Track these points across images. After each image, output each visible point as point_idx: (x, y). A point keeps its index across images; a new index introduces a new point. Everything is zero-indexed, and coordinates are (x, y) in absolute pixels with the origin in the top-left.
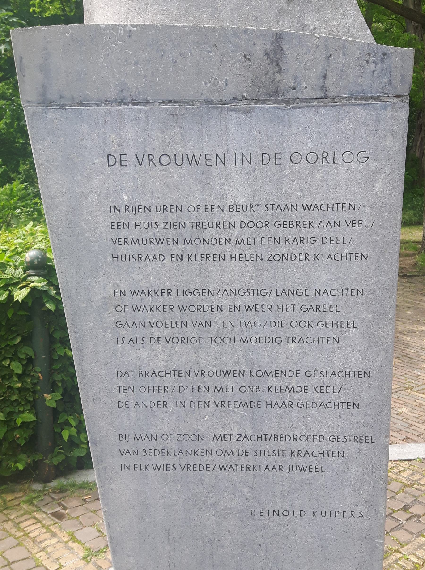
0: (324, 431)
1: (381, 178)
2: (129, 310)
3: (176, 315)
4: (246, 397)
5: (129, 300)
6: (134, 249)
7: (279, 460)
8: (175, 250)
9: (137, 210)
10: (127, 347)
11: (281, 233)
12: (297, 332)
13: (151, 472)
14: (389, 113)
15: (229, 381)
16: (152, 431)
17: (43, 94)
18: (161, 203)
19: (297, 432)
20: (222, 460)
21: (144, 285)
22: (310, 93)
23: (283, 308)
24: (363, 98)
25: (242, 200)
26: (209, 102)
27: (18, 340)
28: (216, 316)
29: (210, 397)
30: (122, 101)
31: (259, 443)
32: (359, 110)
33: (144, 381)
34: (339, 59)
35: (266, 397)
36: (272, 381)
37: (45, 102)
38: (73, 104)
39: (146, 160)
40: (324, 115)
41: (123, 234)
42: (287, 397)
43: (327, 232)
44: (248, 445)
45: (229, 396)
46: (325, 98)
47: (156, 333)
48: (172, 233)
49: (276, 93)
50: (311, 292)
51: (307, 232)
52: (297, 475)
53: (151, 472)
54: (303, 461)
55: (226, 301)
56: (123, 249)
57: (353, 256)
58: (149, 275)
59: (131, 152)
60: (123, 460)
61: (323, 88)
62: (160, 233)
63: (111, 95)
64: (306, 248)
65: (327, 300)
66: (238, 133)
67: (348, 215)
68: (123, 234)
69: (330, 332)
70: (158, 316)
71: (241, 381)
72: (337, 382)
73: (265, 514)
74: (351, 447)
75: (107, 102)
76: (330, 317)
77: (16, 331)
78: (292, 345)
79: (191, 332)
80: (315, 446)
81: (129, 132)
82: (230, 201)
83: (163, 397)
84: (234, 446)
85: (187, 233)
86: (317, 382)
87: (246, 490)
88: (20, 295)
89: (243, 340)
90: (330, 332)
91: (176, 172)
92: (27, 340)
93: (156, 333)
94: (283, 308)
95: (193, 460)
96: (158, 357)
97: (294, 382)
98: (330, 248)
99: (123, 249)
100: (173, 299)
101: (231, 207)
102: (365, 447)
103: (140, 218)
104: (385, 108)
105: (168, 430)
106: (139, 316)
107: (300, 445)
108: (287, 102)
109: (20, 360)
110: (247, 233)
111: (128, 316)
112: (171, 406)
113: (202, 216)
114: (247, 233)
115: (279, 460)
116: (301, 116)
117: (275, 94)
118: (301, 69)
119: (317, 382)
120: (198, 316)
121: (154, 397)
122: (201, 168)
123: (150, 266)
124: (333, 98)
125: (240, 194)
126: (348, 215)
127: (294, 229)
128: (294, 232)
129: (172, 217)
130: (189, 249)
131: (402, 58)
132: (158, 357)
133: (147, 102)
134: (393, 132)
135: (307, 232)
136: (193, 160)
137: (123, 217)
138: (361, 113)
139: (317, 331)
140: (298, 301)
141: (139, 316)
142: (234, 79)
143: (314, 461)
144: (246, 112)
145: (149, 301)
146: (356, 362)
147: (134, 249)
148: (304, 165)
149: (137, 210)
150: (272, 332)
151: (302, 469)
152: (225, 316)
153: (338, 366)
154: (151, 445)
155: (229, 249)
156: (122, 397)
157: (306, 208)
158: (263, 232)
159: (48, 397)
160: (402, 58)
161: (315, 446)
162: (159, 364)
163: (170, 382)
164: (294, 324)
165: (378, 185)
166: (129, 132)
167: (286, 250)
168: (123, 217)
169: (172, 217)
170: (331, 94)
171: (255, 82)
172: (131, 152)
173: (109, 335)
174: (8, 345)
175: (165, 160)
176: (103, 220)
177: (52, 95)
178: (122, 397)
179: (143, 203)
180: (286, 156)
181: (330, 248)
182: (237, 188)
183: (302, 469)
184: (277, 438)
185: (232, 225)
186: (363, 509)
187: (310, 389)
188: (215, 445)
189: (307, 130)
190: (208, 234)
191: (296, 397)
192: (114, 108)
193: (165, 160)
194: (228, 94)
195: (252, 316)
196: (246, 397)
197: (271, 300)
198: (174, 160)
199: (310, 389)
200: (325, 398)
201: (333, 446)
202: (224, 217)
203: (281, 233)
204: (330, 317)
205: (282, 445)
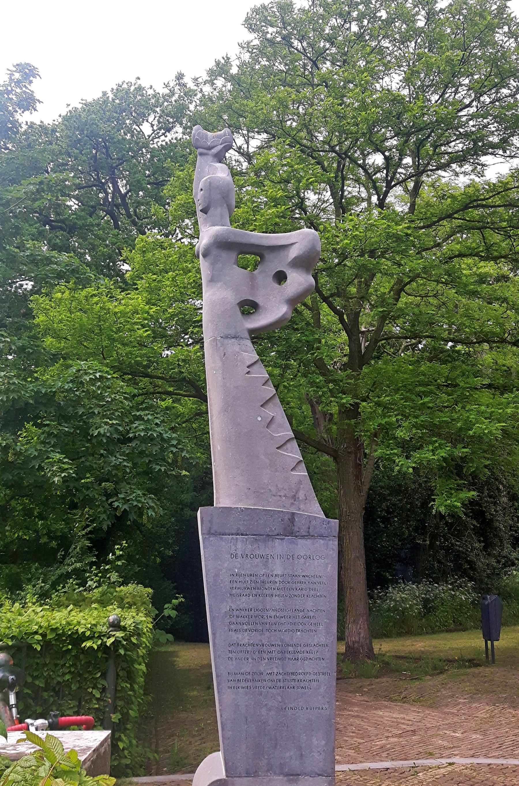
0: (311, 671)
1: (330, 566)
2: (235, 617)
5: (236, 613)
6: (239, 591)
9: (240, 576)
10: (233, 633)
12: (300, 627)
13: (240, 690)
14: (331, 542)
15: (273, 648)
16: (242, 671)
17: (209, 531)
18: (250, 573)
19: (300, 671)
20: (270, 684)
21: (241, 607)
23: (295, 617)
24: (321, 536)
25: (280, 573)
26: (268, 535)
27: (99, 675)
29: (265, 656)
30: (238, 534)
34: (314, 523)
35: (288, 656)
36: (291, 649)
38: (220, 535)
39: (245, 556)
43: (311, 586)
44: (281, 677)
46: (308, 536)
47: (245, 627)
49: (292, 533)
51: (303, 586)
52: (300, 690)
53: (240, 690)
54: (302, 684)
55: (273, 614)
56: (234, 592)
57: (321, 596)
58: (244, 602)
60: (229, 684)
61: (308, 532)
63: (233, 532)
65: (311, 614)
66: (279, 547)
67: (318, 580)
73: (287, 709)
74: (322, 678)
75: (232, 534)
76: (312, 621)
77: (99, 668)
78: (299, 633)
79: (259, 627)
80: (308, 677)
81: (239, 546)
82: (275, 573)
84: (274, 677)
87: (279, 698)
88: (109, 642)
89: (280, 631)
92: (104, 676)
94: (295, 617)
95: (259, 684)
96: (244, 638)
97: (299, 649)
99: (234, 592)
101: (276, 575)
102: (327, 677)
103: (241, 579)
104: (330, 540)
105: (248, 671)
106: (240, 620)
107: (301, 677)
108: (296, 537)
109: (98, 689)
111: (234, 620)
112: (250, 659)
116: (301, 541)
117: (292, 534)
118: (300, 525)
123: (244, 599)
124: (312, 536)
125: (279, 571)
126: (318, 580)
127: (299, 584)
129: (253, 578)
131: (335, 523)
132: (244, 638)
133: (247, 535)
134: (333, 550)
135: (303, 586)
136: (262, 557)
137: (235, 578)
138: (322, 542)
139: (308, 627)
140: (301, 614)
141: (240, 620)
142: (277, 527)
143: (307, 684)
144: (282, 539)
145: (243, 613)
146: (323, 640)
147: (239, 591)
148: (302, 560)
149: (240, 576)
150: (290, 627)
152: (273, 620)
153: (316, 641)
154: (241, 677)
156: (230, 655)
157: (304, 576)
159: (113, 716)
160: (335, 523)
163: (249, 648)
165: (329, 569)
166: (239, 546)
168: (235, 578)
169: (253, 578)
170: (312, 534)
171: (285, 529)
173: (226, 628)
174: (93, 678)
175: (252, 556)
176: (227, 579)
177: (212, 531)
178: (230, 655)
179: (243, 573)
180: (296, 556)
184: (293, 674)
185: (276, 582)
186: (327, 706)
188: (267, 677)
189: (303, 546)
192: (234, 537)
193: (252, 556)
194: (276, 532)
195: (283, 620)
198: (255, 556)
200: (311, 656)
202: (273, 579)
204: (312, 621)
205: (294, 677)
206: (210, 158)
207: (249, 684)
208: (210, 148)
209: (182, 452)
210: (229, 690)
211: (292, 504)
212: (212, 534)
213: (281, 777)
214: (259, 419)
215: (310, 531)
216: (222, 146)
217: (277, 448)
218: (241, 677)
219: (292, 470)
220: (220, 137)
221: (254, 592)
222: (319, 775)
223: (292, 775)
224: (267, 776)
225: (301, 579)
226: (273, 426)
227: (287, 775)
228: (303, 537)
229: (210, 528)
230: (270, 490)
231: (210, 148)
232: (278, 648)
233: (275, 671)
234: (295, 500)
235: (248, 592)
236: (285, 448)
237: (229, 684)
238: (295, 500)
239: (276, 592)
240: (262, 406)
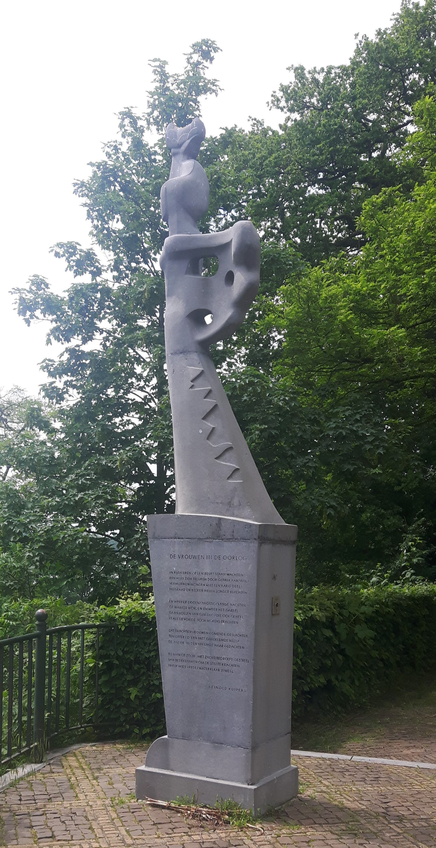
3: (188, 610)
4: (208, 642)
7: (218, 667)
8: (188, 587)
9: (177, 573)
11: (220, 583)
12: (225, 619)
15: (203, 635)
16: (179, 652)
17: (154, 535)
19: (224, 657)
20: (200, 665)
22: (229, 537)
24: (244, 539)
26: (199, 539)
28: (200, 611)
29: (197, 641)
30: (175, 538)
31: (212, 660)
32: (243, 543)
33: (177, 634)
36: (216, 637)
37: (155, 538)
40: (233, 544)
41: (173, 581)
42: (221, 643)
45: (203, 641)
46: (232, 539)
47: (181, 616)
48: (187, 581)
50: (229, 605)
51: (227, 583)
54: (226, 668)
56: (173, 586)
58: (179, 596)
59: (177, 554)
60: (170, 663)
62: (184, 581)
64: (228, 588)
65: (234, 608)
66: (207, 549)
68: (173, 581)
69: (235, 620)
70: (182, 610)
71: (207, 636)
72: (237, 638)
75: (171, 538)
76: (235, 614)
78: (223, 624)
79: (192, 617)
80: (230, 662)
82: (205, 571)
83: (183, 640)
85: (192, 582)
86: (230, 638)
90: (235, 620)
91: (190, 561)
93: (181, 616)
95: (191, 664)
97: (224, 637)
98: (235, 589)
99: (173, 586)
100: (186, 605)
102: (246, 664)
104: (251, 542)
106: (177, 610)
107: (225, 661)
108: (222, 540)
110: (210, 582)
111: (173, 610)
113: (196, 576)
114: (210, 582)
115: (218, 667)
116: (226, 544)
117: (218, 537)
119: (230, 638)
120: (195, 611)
121: (180, 640)
122: (197, 560)
123: (181, 592)
128: (224, 583)
129: (188, 576)
130: (192, 587)
133: (182, 538)
135: (227, 583)
136: (194, 557)
137: (174, 575)
138: (244, 544)
139: (230, 619)
140: (225, 607)
141: (177, 610)
144: (210, 542)
149: (177, 573)
151: (226, 671)
154: (178, 658)
155: (205, 588)
156: (170, 639)
158: (215, 582)
161: (230, 662)
162: (181, 628)
163: (185, 634)
164: (225, 557)
167: (222, 589)
168: (174, 575)
169: (188, 576)
172: (177, 554)
175: (187, 557)
177: (156, 536)
178: (170, 639)
181: (235, 589)
182: (207, 567)
183: (226, 671)
187: (228, 640)
188: (198, 659)
189: (228, 548)
190: (198, 582)
191: (224, 643)
193: (187, 557)
195: (210, 612)
196: (208, 642)
197: (216, 606)
199: (228, 640)
200: (234, 644)
201: (236, 663)
202: (203, 576)
203: (220, 583)
204: (235, 614)
205: (219, 661)
206: (181, 157)
207: (184, 664)
208: (180, 146)
209: (378, 449)
210: (170, 667)
211: (228, 510)
212: (156, 538)
213: (208, 744)
214: (201, 432)
215: (235, 534)
216: (189, 141)
217: (217, 458)
218: (178, 658)
219: (228, 478)
220: (189, 129)
221: (188, 587)
222: (239, 747)
223: (217, 743)
224: (198, 741)
225: (226, 577)
226: (214, 437)
227: (214, 742)
228: (228, 540)
229: (154, 533)
230: (209, 498)
231: (180, 146)
232: (207, 636)
233: (205, 655)
234: (230, 507)
235: (183, 587)
236: (224, 457)
237: (170, 663)
238: (230, 507)
239: (205, 588)
240: (204, 418)
